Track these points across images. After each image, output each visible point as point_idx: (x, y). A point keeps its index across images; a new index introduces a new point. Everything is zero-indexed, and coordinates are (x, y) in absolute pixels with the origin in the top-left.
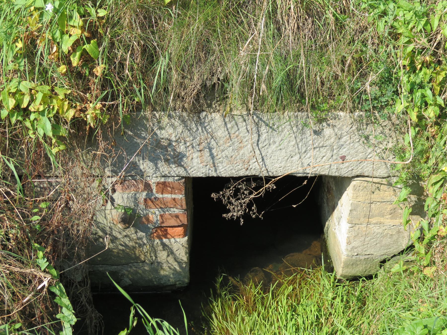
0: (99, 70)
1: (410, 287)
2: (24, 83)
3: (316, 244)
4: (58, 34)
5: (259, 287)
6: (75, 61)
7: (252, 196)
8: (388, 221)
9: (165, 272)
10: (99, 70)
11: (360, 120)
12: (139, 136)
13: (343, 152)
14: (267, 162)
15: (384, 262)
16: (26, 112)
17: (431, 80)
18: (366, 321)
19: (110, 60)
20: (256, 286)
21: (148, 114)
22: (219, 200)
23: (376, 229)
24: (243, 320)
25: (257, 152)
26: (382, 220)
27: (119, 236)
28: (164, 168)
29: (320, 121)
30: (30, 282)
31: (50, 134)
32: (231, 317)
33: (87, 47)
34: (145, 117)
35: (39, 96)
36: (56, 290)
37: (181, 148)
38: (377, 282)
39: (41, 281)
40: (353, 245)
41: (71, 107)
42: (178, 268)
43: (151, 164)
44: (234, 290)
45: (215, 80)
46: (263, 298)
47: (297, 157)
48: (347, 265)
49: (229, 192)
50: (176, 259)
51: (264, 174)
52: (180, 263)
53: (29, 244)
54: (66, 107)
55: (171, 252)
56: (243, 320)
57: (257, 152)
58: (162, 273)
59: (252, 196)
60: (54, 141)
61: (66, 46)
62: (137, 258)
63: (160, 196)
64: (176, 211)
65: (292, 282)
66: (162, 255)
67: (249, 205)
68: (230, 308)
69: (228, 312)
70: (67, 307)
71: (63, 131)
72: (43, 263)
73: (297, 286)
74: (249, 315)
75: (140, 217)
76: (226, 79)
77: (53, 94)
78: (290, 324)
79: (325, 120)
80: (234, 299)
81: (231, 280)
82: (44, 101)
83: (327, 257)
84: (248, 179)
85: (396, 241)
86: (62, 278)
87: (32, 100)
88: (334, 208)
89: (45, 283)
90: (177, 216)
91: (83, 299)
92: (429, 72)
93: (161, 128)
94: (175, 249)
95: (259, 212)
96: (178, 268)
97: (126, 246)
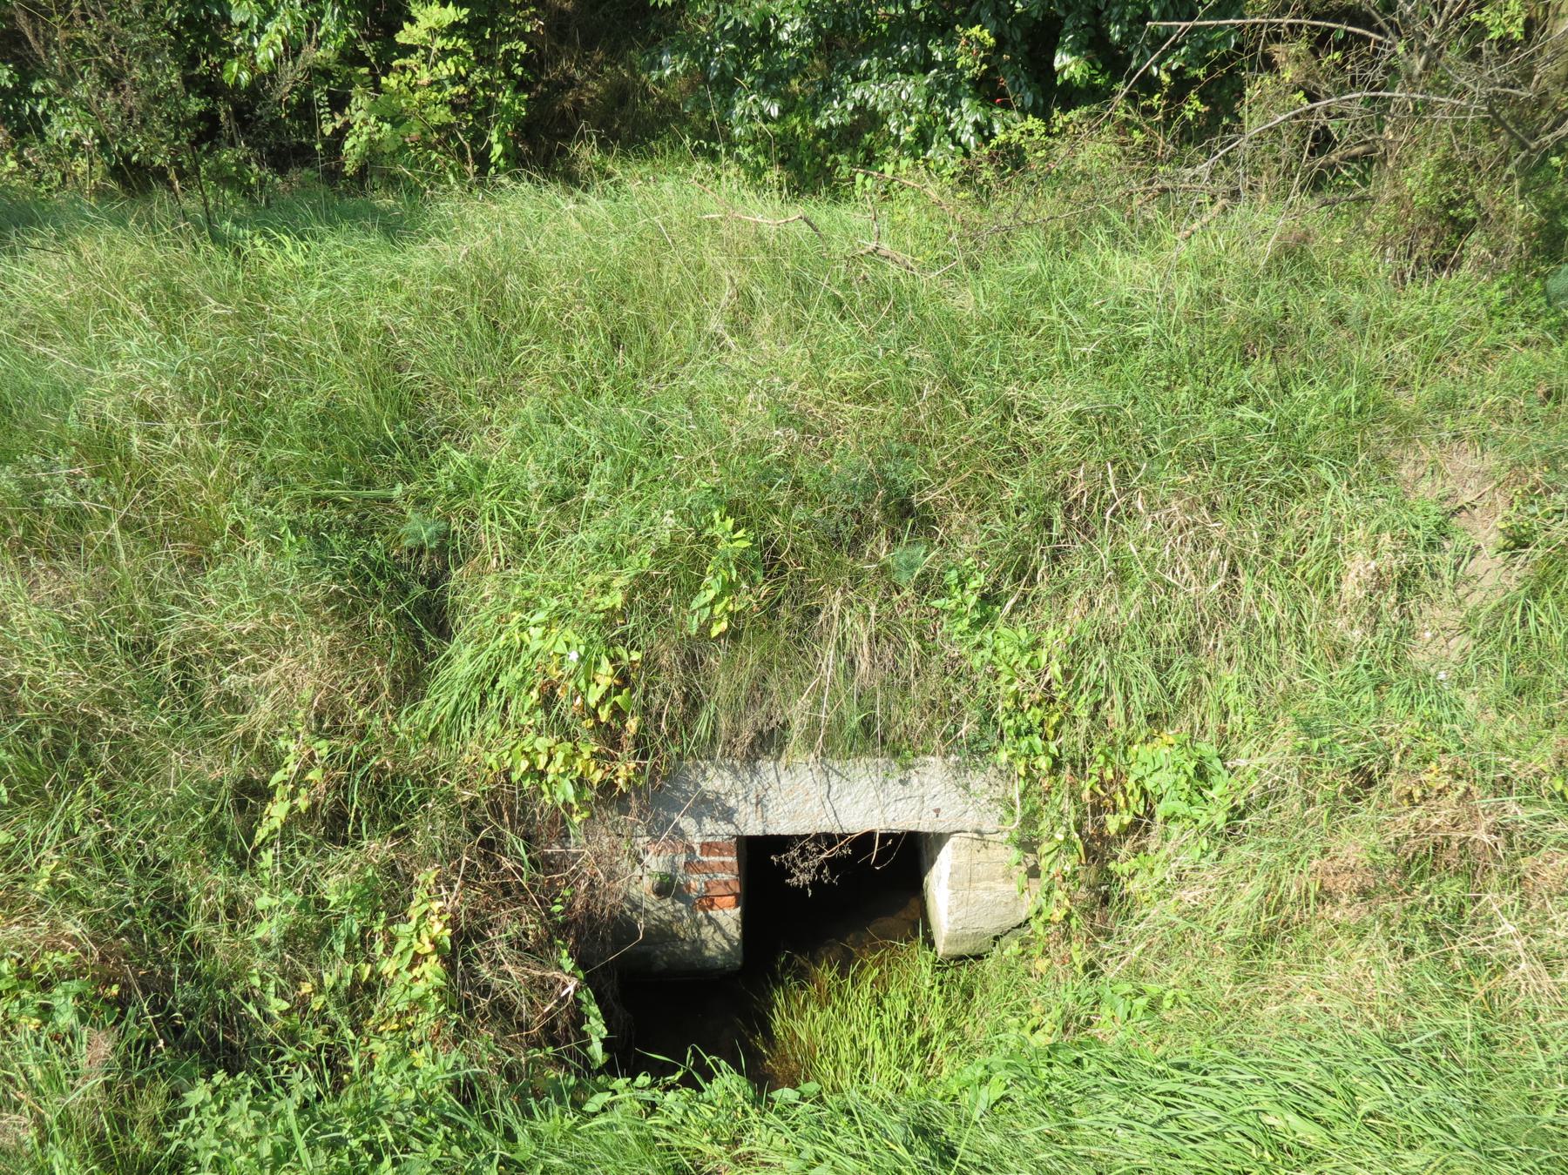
0: (632, 724)
1: (888, 1112)
2: (541, 740)
3: (914, 902)
4: (582, 683)
5: (835, 969)
6: (604, 715)
7: (823, 856)
8: (1001, 886)
9: (711, 951)
10: (632, 724)
11: (957, 766)
12: (679, 790)
13: (936, 804)
14: (841, 817)
15: (996, 938)
16: (543, 775)
17: (1041, 724)
18: (971, 1021)
19: (645, 710)
20: (831, 968)
21: (690, 762)
22: (781, 865)
23: (986, 896)
24: (813, 1017)
25: (828, 805)
26: (992, 884)
27: (652, 909)
28: (709, 825)
29: (906, 767)
30: (551, 987)
31: (572, 800)
32: (798, 1013)
33: (618, 699)
34: (686, 767)
35: (560, 757)
36: (583, 997)
37: (732, 802)
38: (989, 963)
39: (565, 986)
40: (956, 915)
41: (598, 767)
42: (727, 947)
43: (693, 821)
44: (803, 976)
45: (773, 724)
46: (840, 985)
47: (877, 812)
48: (949, 942)
49: (794, 853)
50: (725, 936)
51: (837, 831)
52: (729, 941)
53: (550, 940)
54: (592, 768)
55: (719, 928)
56: (813, 1017)
57: (828, 805)
58: (707, 953)
59: (823, 856)
60: (576, 807)
61: (592, 700)
62: (675, 936)
63: (705, 859)
64: (726, 877)
65: (880, 962)
66: (707, 932)
67: (819, 870)
68: (796, 1000)
69: (794, 1007)
70: (595, 1016)
71: (589, 795)
72: (568, 964)
73: (885, 967)
74: (821, 1011)
75: (679, 885)
76: (785, 726)
77: (577, 751)
78: (873, 1027)
79: (911, 767)
80: (802, 987)
81: (799, 960)
82: (565, 762)
83: (927, 925)
84: (817, 838)
85: (1014, 911)
86: (589, 981)
87: (550, 758)
88: (933, 862)
89: (571, 988)
90: (726, 883)
91: (609, 995)
92: (1039, 711)
93: (705, 779)
94: (723, 924)
95: (833, 876)
96: (727, 947)
97: (661, 920)
